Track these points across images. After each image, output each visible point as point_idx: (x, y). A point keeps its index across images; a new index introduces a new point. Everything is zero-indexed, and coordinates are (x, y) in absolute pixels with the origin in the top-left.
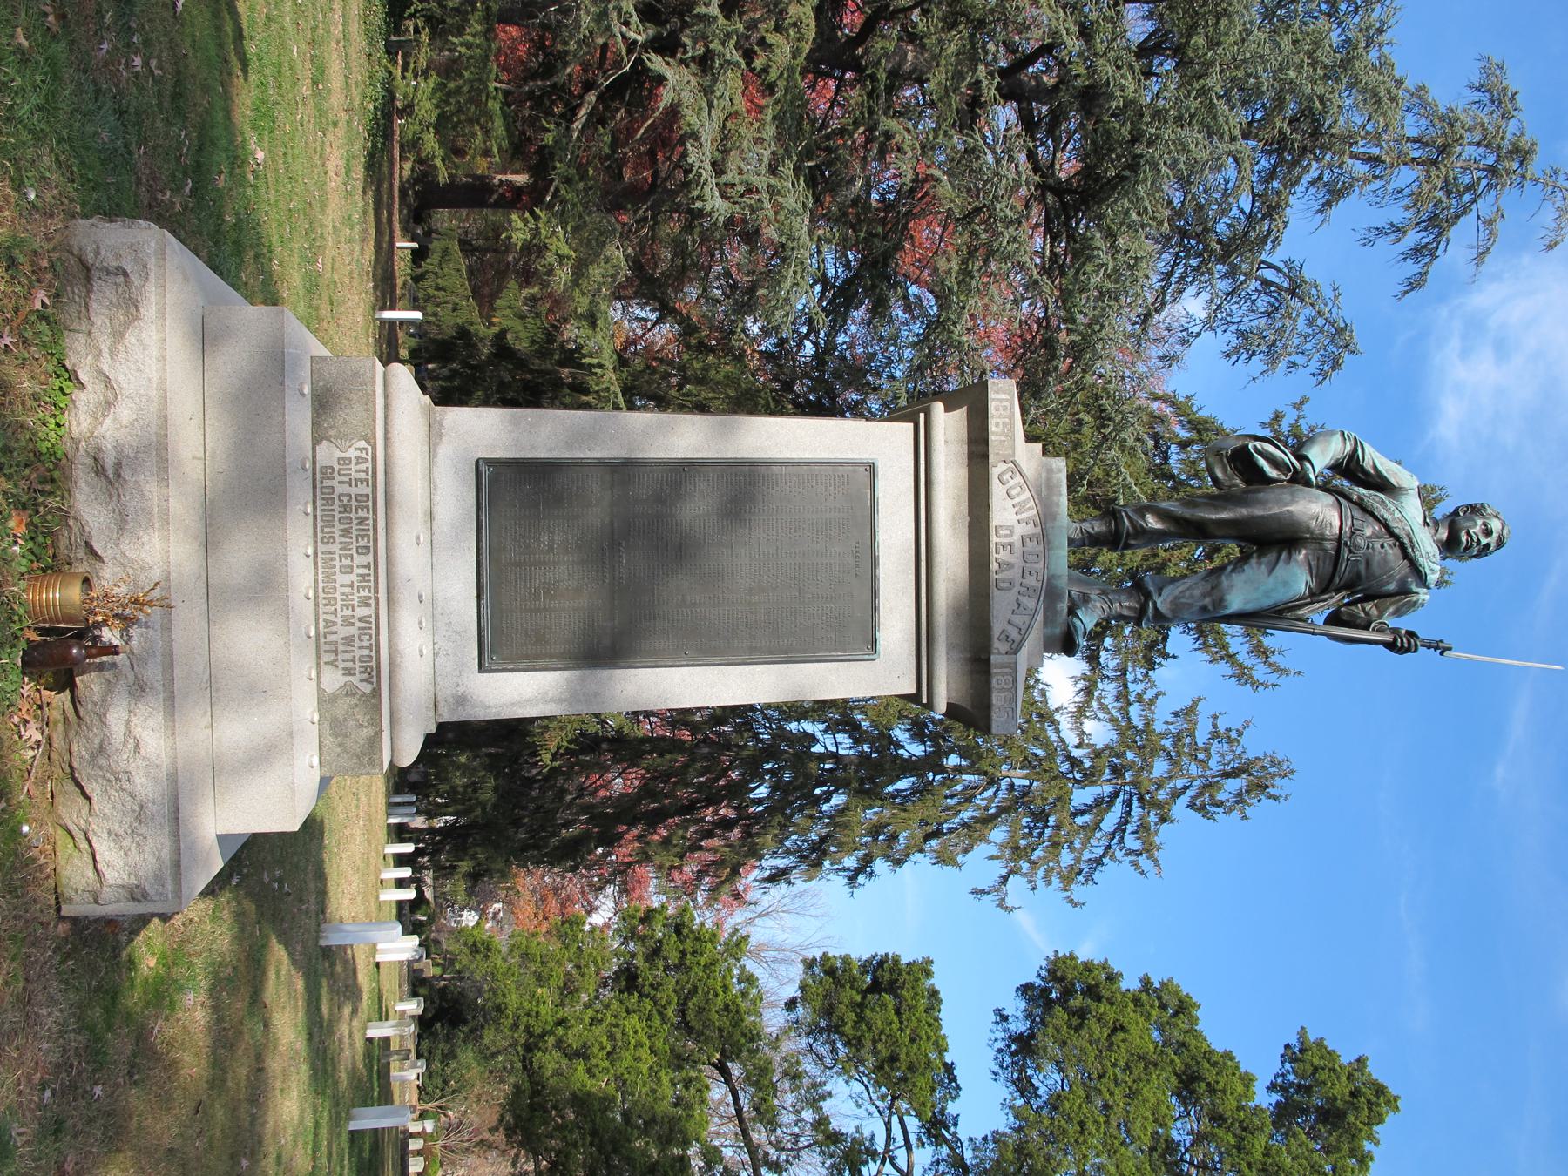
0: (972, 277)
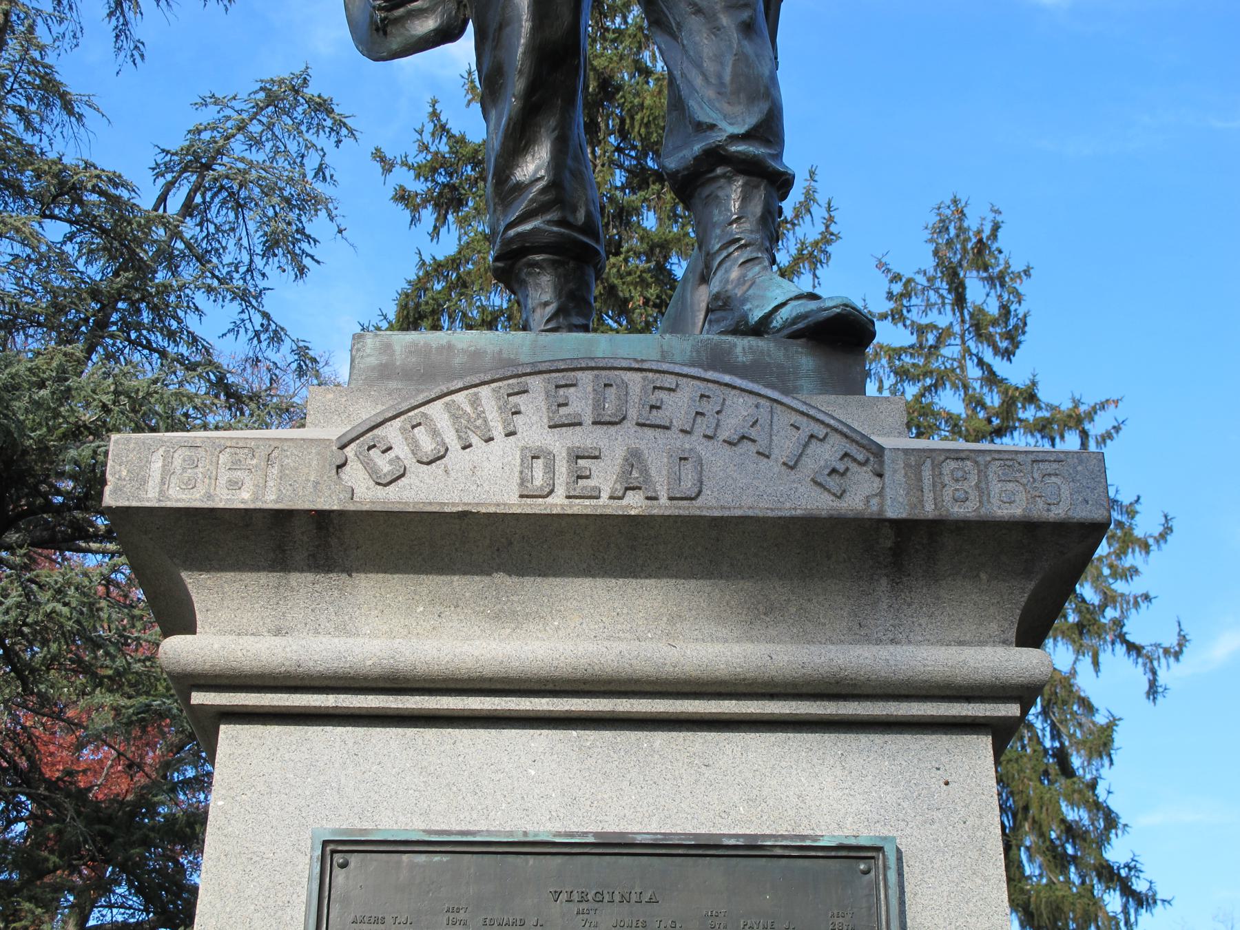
0: (128, 669)
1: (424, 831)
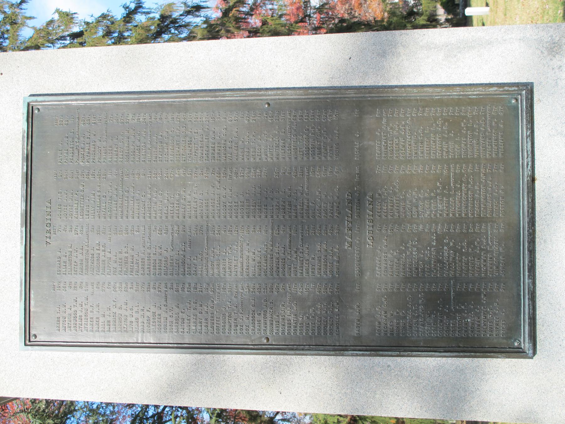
1: (20, 301)
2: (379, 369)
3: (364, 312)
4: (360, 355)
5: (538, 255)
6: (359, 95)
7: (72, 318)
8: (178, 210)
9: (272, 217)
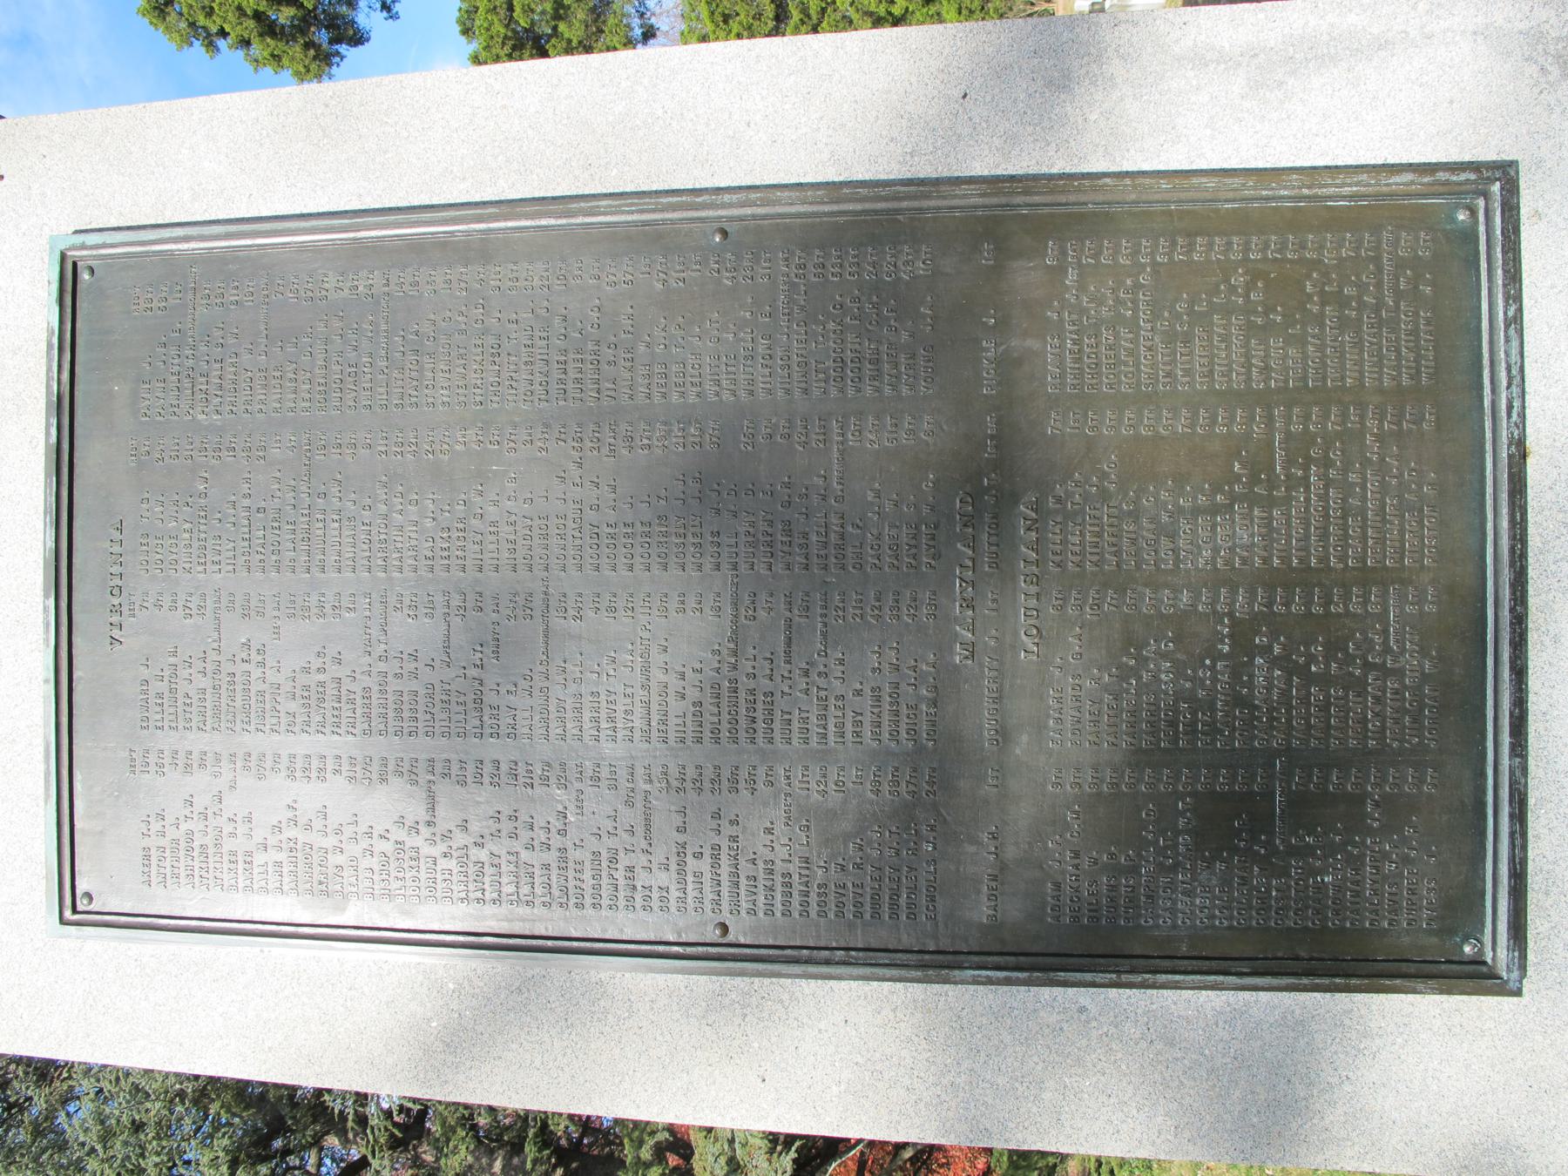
2: (1054, 1018)
3: (1011, 853)
4: (999, 982)
5: (1534, 682)
6: (995, 200)
7: (182, 852)
8: (463, 549)
9: (735, 567)
